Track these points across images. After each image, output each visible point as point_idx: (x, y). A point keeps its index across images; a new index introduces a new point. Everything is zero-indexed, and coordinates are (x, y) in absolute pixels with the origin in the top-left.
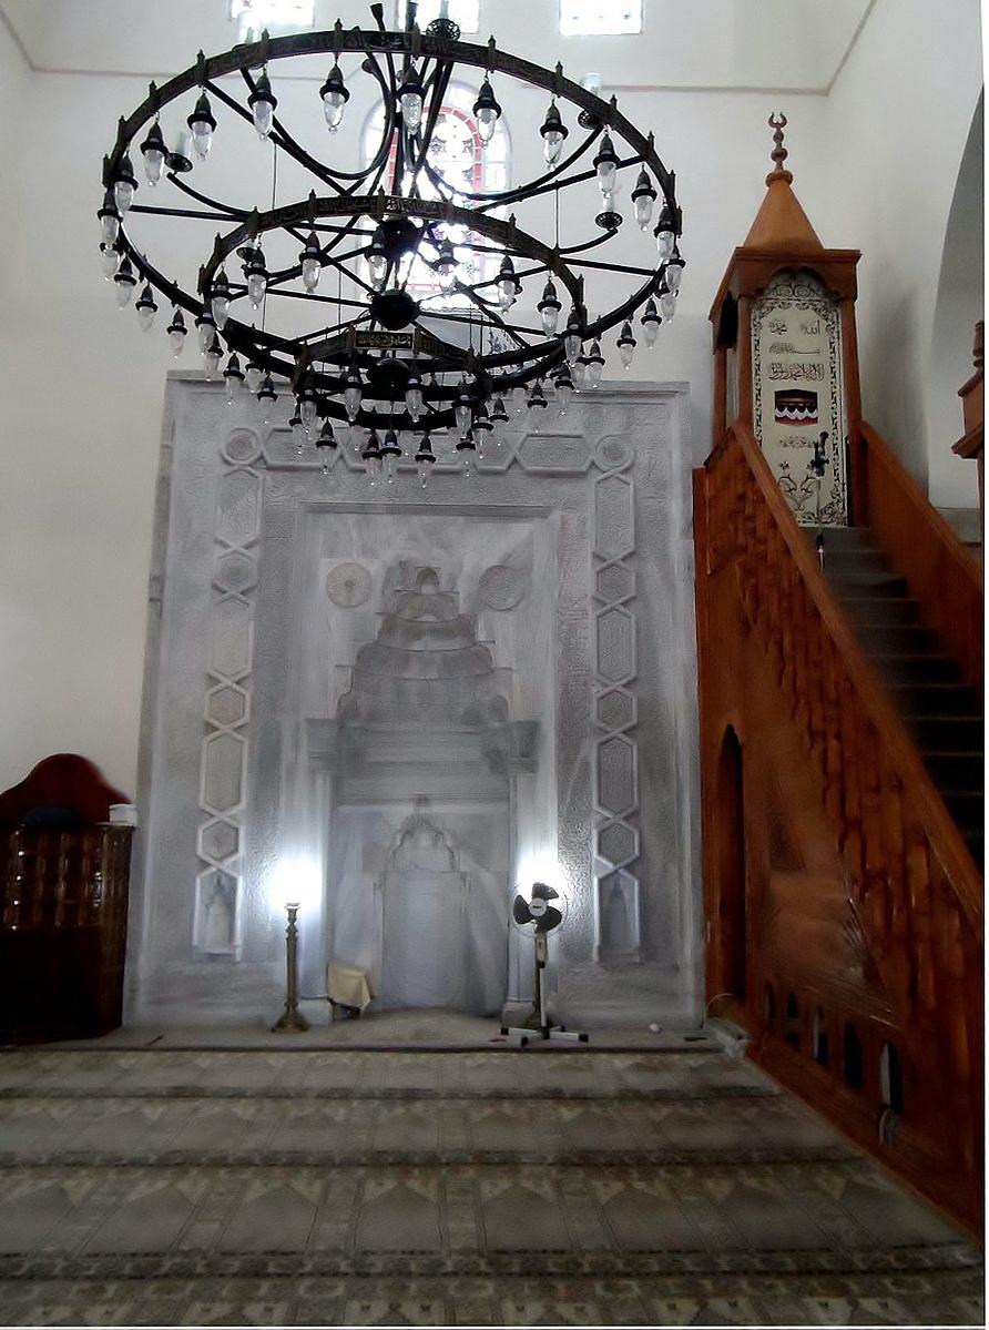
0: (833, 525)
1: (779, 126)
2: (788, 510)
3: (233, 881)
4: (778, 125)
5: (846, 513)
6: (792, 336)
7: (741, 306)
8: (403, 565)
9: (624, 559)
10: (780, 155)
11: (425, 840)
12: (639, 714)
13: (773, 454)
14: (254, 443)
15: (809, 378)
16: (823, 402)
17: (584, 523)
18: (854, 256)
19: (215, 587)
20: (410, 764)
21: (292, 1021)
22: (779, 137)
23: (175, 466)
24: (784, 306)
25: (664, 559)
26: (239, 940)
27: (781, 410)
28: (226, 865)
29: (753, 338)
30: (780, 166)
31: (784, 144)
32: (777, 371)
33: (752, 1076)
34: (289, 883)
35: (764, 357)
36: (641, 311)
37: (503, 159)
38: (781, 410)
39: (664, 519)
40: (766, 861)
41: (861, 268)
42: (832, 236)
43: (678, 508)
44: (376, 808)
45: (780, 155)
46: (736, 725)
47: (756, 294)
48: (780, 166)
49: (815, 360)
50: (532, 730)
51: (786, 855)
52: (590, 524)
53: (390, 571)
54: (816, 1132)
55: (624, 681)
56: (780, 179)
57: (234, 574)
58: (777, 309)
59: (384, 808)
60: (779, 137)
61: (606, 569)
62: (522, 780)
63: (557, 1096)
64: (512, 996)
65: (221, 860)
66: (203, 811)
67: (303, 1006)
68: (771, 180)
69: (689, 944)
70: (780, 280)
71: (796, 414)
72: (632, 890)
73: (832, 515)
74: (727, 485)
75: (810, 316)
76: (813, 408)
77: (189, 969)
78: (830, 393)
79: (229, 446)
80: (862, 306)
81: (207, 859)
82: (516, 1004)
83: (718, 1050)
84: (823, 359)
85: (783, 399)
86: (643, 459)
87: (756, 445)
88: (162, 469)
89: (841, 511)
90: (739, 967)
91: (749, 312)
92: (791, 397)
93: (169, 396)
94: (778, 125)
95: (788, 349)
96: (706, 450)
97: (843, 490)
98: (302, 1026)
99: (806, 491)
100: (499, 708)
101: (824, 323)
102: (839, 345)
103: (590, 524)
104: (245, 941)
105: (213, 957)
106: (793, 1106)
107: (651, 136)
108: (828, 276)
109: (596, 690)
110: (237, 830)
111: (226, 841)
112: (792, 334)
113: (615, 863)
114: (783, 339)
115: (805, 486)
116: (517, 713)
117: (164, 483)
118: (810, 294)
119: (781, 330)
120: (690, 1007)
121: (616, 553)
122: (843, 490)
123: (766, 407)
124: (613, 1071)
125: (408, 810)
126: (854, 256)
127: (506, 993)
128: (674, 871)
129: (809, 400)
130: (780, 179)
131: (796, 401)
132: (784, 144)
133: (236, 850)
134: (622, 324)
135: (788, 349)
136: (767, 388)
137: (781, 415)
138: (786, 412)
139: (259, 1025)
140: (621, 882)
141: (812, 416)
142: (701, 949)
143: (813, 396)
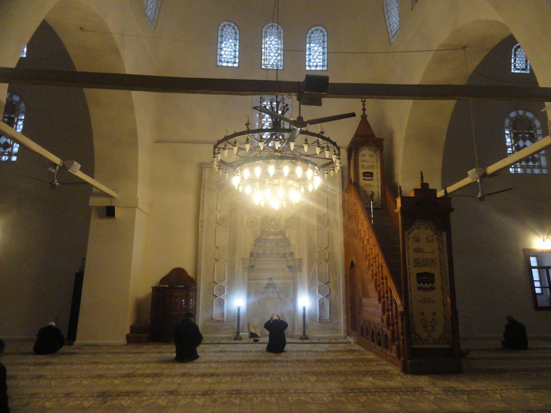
2: (388, 31)
3: (223, 301)
11: (271, 290)
16: (375, 174)
18: (383, 140)
20: (267, 269)
21: (238, 338)
26: (225, 317)
28: (222, 297)
33: (357, 347)
34: (238, 302)
37: (278, 80)
40: (361, 295)
44: (258, 281)
46: (354, 260)
50: (301, 260)
51: (366, 295)
54: (371, 356)
59: (260, 281)
60: (364, 105)
62: (299, 274)
63: (311, 351)
64: (296, 330)
65: (220, 295)
66: (215, 282)
67: (241, 334)
69: (342, 318)
71: (368, 178)
76: (372, 177)
77: (212, 324)
83: (350, 343)
85: (365, 174)
90: (356, 323)
98: (241, 339)
100: (292, 254)
101: (375, 154)
104: (227, 317)
105: (218, 321)
106: (367, 352)
109: (318, 249)
111: (222, 290)
113: (323, 295)
114: (365, 158)
116: (297, 256)
119: (364, 156)
120: (342, 334)
123: (361, 177)
124: (323, 348)
125: (267, 282)
126: (383, 140)
128: (338, 297)
129: (371, 174)
132: (366, 107)
133: (224, 293)
136: (361, 171)
139: (230, 338)
142: (345, 318)
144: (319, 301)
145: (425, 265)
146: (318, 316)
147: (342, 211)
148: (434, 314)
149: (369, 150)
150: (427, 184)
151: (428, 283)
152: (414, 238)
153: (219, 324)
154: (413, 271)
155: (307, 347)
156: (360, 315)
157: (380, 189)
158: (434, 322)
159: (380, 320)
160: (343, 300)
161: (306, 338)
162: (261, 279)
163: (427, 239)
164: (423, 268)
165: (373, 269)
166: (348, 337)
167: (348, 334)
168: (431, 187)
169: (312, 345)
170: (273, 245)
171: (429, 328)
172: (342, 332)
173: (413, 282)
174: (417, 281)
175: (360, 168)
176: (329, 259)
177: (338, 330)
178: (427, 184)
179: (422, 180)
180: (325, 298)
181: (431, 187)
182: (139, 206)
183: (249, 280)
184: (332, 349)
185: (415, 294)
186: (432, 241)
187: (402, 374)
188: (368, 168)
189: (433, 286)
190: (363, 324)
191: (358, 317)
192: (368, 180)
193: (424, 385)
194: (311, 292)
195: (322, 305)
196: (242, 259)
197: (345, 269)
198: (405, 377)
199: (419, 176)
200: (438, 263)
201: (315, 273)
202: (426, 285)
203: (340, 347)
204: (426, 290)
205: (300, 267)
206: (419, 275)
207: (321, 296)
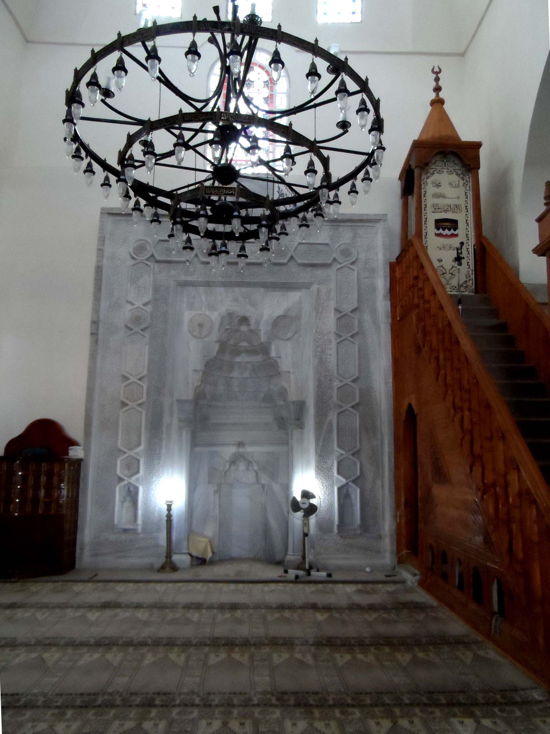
0: (467, 293)
1: (437, 73)
3: (136, 489)
4: (437, 73)
5: (474, 287)
6: (445, 189)
7: (416, 172)
10: (438, 89)
11: (242, 466)
14: (148, 247)
15: (453, 212)
16: (461, 225)
19: (127, 327)
21: (169, 566)
22: (437, 80)
24: (440, 172)
25: (374, 311)
26: (140, 521)
28: (133, 480)
30: (438, 95)
31: (440, 83)
33: (421, 596)
34: (167, 490)
35: (429, 201)
36: (361, 175)
39: (373, 289)
42: (466, 135)
43: (381, 284)
44: (215, 449)
45: (438, 89)
47: (424, 166)
48: (438, 95)
49: (457, 202)
50: (301, 406)
51: (441, 475)
53: (223, 318)
55: (351, 379)
56: (438, 103)
57: (137, 320)
60: (437, 80)
61: (342, 317)
63: (314, 607)
64: (290, 552)
66: (120, 450)
68: (433, 103)
69: (387, 524)
70: (438, 158)
71: (447, 232)
73: (466, 287)
74: (408, 270)
75: (454, 178)
76: (456, 228)
80: (481, 172)
81: (122, 476)
83: (403, 582)
85: (439, 224)
86: (362, 256)
88: (98, 262)
90: (415, 537)
91: (420, 175)
93: (102, 221)
94: (437, 73)
95: (442, 196)
96: (397, 251)
97: (472, 274)
98: (174, 568)
101: (461, 182)
102: (470, 194)
104: (144, 522)
105: (125, 531)
106: (445, 613)
107: (367, 79)
108: (464, 156)
112: (444, 188)
117: (99, 269)
118: (454, 165)
120: (387, 558)
121: (347, 308)
123: (430, 228)
124: (345, 594)
125: (233, 450)
126: (477, 146)
128: (379, 482)
129: (453, 224)
130: (438, 103)
131: (447, 225)
133: (138, 472)
134: (349, 184)
135: (442, 196)
139: (150, 568)
141: (456, 233)
144: (339, 489)
145: (446, 211)
147: (389, 303)
149: (450, 173)
153: (128, 538)
159: (479, 539)
160: (390, 489)
165: (462, 418)
167: (401, 561)
170: (247, 375)
175: (429, 209)
176: (364, 403)
180: (350, 484)
184: (364, 600)
192: (446, 236)
194: (322, 470)
196: (179, 401)
197: (395, 424)
201: (330, 431)
203: (381, 595)
205: (299, 421)
207: (344, 481)
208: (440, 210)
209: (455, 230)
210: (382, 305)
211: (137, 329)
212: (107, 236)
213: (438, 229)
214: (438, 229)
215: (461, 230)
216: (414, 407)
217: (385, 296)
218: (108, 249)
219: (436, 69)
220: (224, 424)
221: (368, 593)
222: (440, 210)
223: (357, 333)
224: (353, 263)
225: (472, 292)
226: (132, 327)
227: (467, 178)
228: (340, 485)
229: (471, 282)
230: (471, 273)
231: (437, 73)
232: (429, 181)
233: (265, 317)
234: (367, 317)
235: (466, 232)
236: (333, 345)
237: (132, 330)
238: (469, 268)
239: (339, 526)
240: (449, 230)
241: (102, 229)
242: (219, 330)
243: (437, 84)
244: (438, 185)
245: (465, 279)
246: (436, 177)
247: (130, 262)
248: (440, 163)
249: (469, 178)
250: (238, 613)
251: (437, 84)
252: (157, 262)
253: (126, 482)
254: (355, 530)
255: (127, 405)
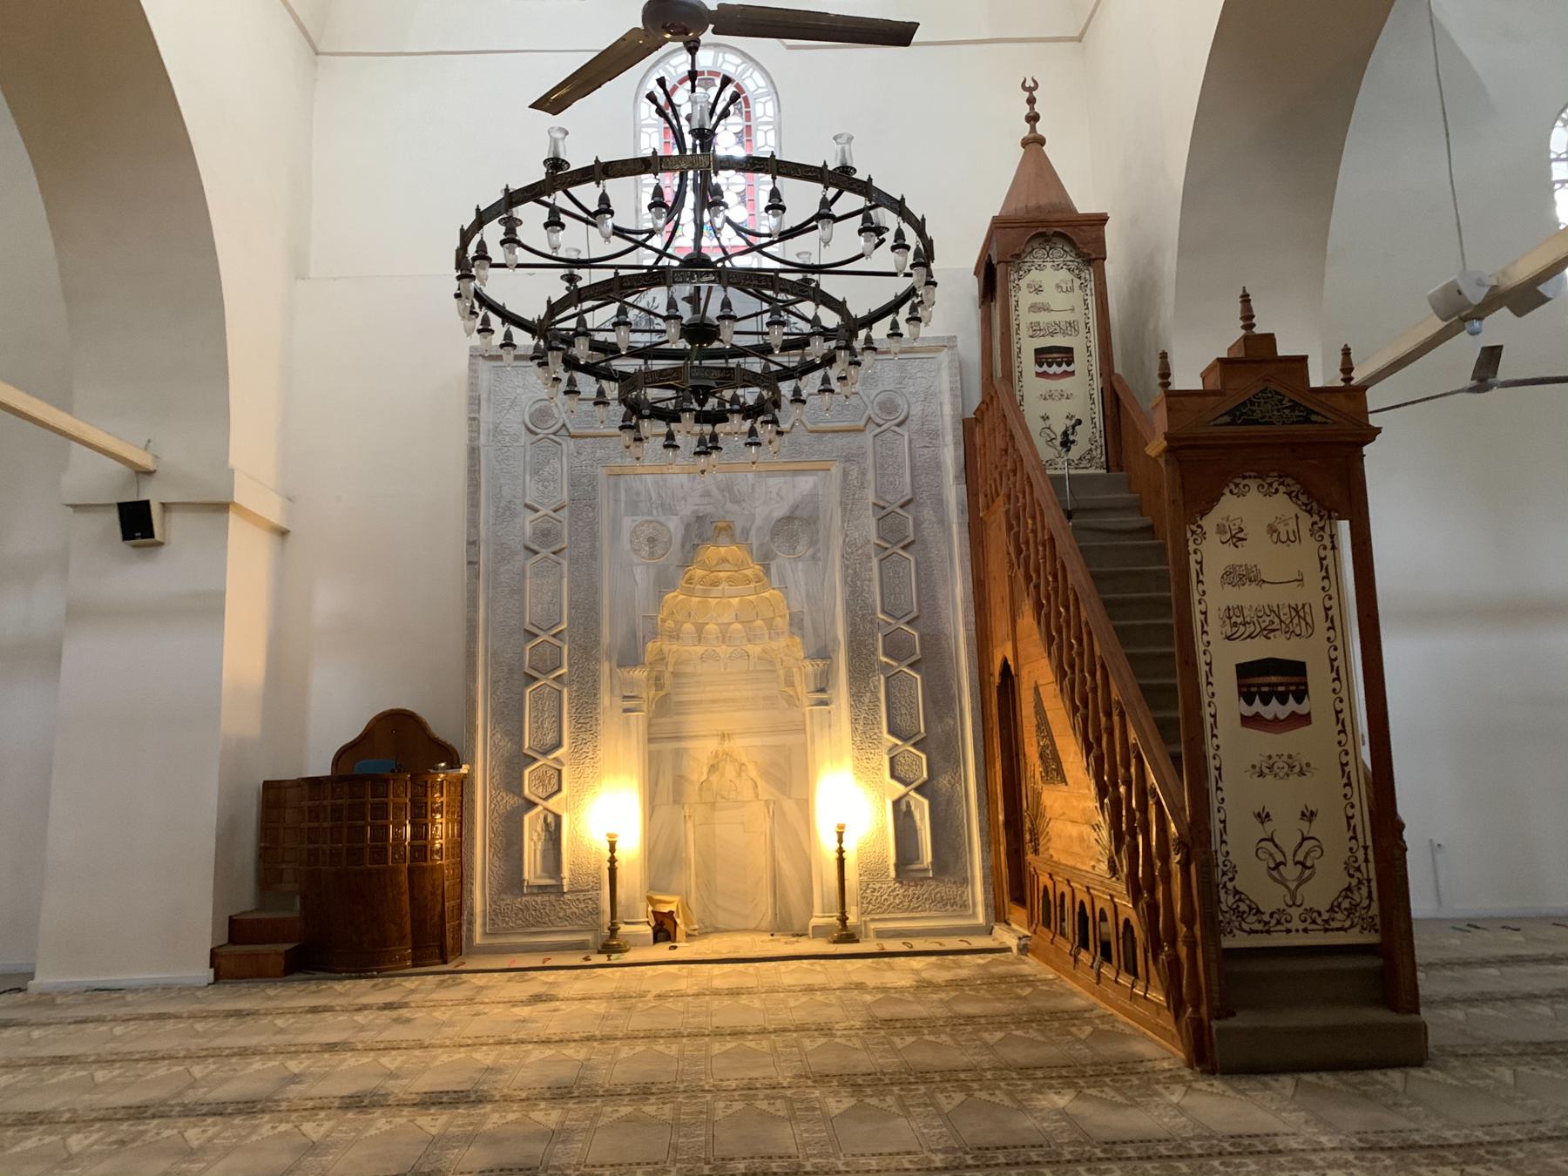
0: (1092, 471)
1: (1030, 90)
4: (1030, 90)
5: (1375, 909)
6: (1050, 296)
7: (1000, 270)
8: (700, 519)
9: (902, 507)
10: (1033, 118)
12: (922, 648)
13: (1033, 409)
14: (555, 411)
15: (1065, 334)
17: (864, 474)
18: (1101, 220)
19: (527, 548)
22: (1031, 101)
23: (483, 439)
24: (1040, 268)
25: (939, 503)
26: (566, 873)
27: (1250, 702)
28: (552, 804)
29: (1192, 558)
30: (1033, 129)
31: (1037, 108)
32: (1036, 330)
35: (1024, 317)
36: (904, 311)
38: (1250, 702)
39: (938, 466)
41: (1109, 229)
42: (1084, 205)
43: (950, 456)
44: (683, 745)
45: (1033, 118)
47: (1015, 259)
48: (1033, 129)
49: (1070, 317)
51: (1054, 772)
52: (870, 476)
53: (688, 527)
55: (907, 618)
56: (1034, 143)
57: (545, 535)
58: (1034, 273)
60: (1031, 101)
61: (884, 515)
64: (817, 911)
66: (527, 756)
68: (1025, 143)
70: (1035, 244)
71: (1055, 369)
72: (922, 810)
73: (1350, 911)
74: (990, 428)
75: (1064, 275)
78: (1084, 345)
79: (531, 416)
80: (1109, 267)
81: (533, 798)
82: (822, 917)
84: (1078, 316)
85: (1042, 355)
86: (916, 411)
87: (1017, 407)
88: (472, 440)
89: (1366, 903)
91: (1007, 275)
92: (1268, 674)
93: (473, 370)
94: (1030, 90)
95: (1045, 308)
96: (976, 399)
97: (1366, 861)
99: (1302, 864)
101: (1077, 282)
102: (1092, 301)
103: (870, 476)
107: (903, 199)
108: (1079, 238)
110: (560, 772)
112: (1048, 292)
115: (1300, 857)
117: (473, 452)
118: (1061, 254)
121: (893, 500)
122: (1366, 861)
125: (712, 745)
126: (1101, 220)
127: (810, 905)
129: (1067, 354)
130: (1034, 143)
131: (1054, 357)
134: (889, 318)
135: (1045, 308)
136: (1027, 346)
137: (1040, 370)
138: (1258, 706)
140: (912, 803)
141: (1070, 369)
143: (1069, 351)
145: (1267, 632)
146: (892, 859)
148: (1308, 816)
149: (1057, 268)
150: (1270, 339)
151: (1283, 701)
152: (1221, 530)
154: (1221, 659)
155: (856, 970)
156: (1036, 851)
157: (1098, 408)
158: (1308, 844)
161: (850, 938)
162: (691, 737)
163: (1272, 530)
164: (1260, 640)
166: (999, 930)
167: (998, 915)
168: (1283, 350)
169: (933, 959)
171: (1291, 872)
172: (980, 910)
173: (1222, 698)
174: (1240, 693)
175: (1024, 332)
177: (964, 906)
178: (1270, 339)
179: (1249, 326)
180: (912, 793)
181: (1283, 350)
182: (239, 497)
183: (651, 740)
185: (1232, 742)
186: (1296, 537)
187: (1186, 1073)
188: (1052, 334)
189: (1302, 709)
190: (1050, 884)
191: (1030, 857)
193: (1279, 1127)
195: (902, 816)
198: (1202, 1085)
199: (1237, 307)
200: (1321, 624)
202: (1274, 709)
204: (1276, 725)
206: (1244, 670)
208: (1250, 629)
209: (1069, 364)
210: (953, 493)
211: (544, 552)
212: (484, 396)
213: (1041, 365)
214: (1041, 365)
215: (1079, 365)
216: (1011, 662)
217: (956, 477)
218: (486, 415)
219: (1029, 84)
220: (701, 702)
221: (948, 968)
222: (1250, 629)
223: (913, 542)
224: (899, 425)
225: (1373, 928)
226: (536, 548)
227: (1085, 274)
228: (896, 797)
229: (1364, 891)
230: (1360, 855)
231: (1030, 90)
232: (1209, 522)
233: (758, 522)
234: (928, 513)
235: (1086, 361)
236: (875, 562)
237: (536, 553)
238: (1354, 837)
239: (897, 866)
240: (1059, 365)
241: (473, 384)
242: (683, 546)
243: (1032, 108)
244: (1038, 290)
245: (1346, 881)
246: (1034, 276)
247: (525, 438)
248: (1040, 253)
249: (1089, 274)
250: (744, 1000)
251: (1032, 108)
252: (573, 437)
253: (540, 808)
254: (926, 870)
255: (536, 679)
